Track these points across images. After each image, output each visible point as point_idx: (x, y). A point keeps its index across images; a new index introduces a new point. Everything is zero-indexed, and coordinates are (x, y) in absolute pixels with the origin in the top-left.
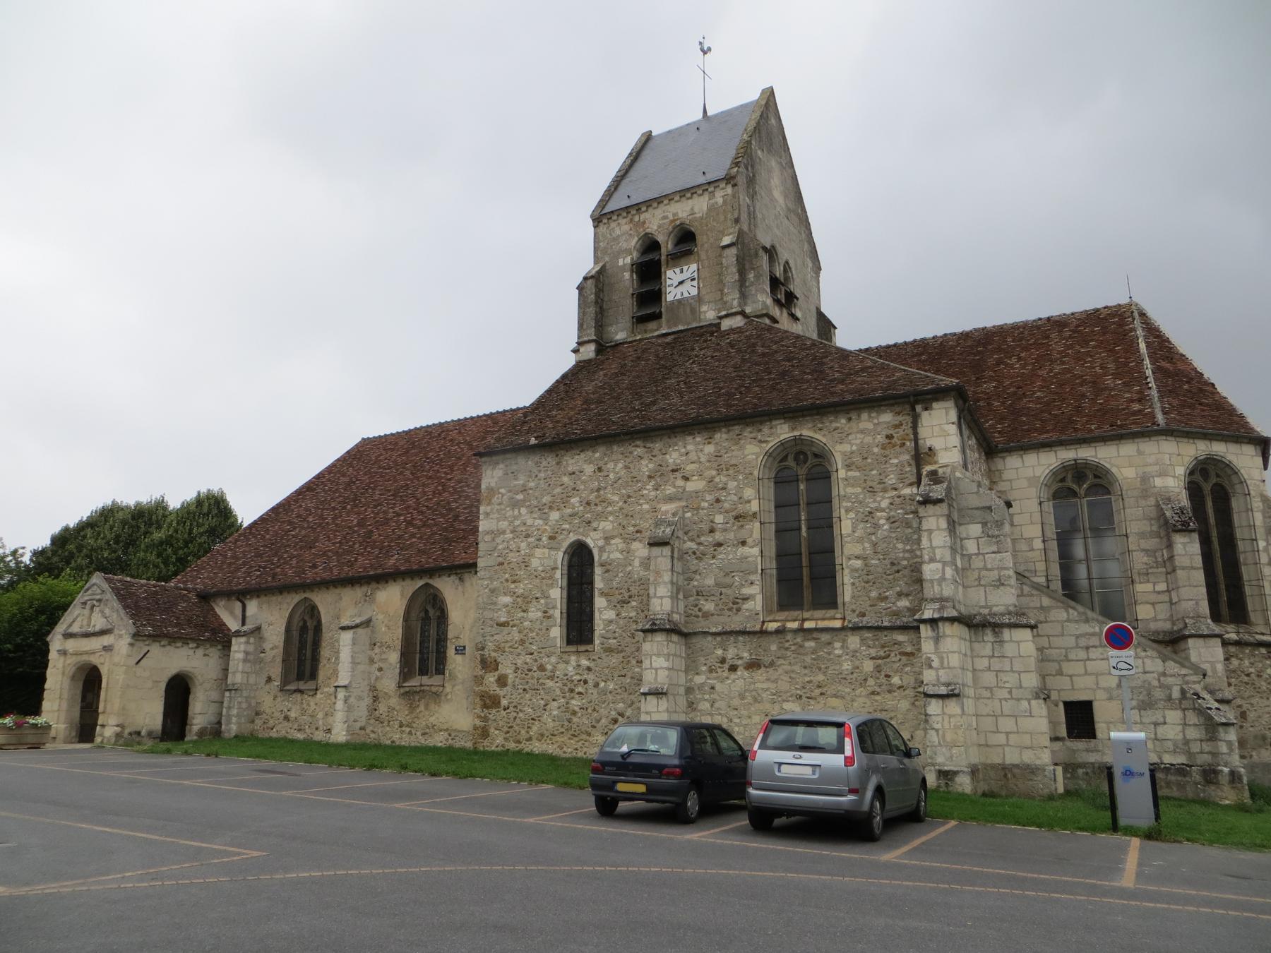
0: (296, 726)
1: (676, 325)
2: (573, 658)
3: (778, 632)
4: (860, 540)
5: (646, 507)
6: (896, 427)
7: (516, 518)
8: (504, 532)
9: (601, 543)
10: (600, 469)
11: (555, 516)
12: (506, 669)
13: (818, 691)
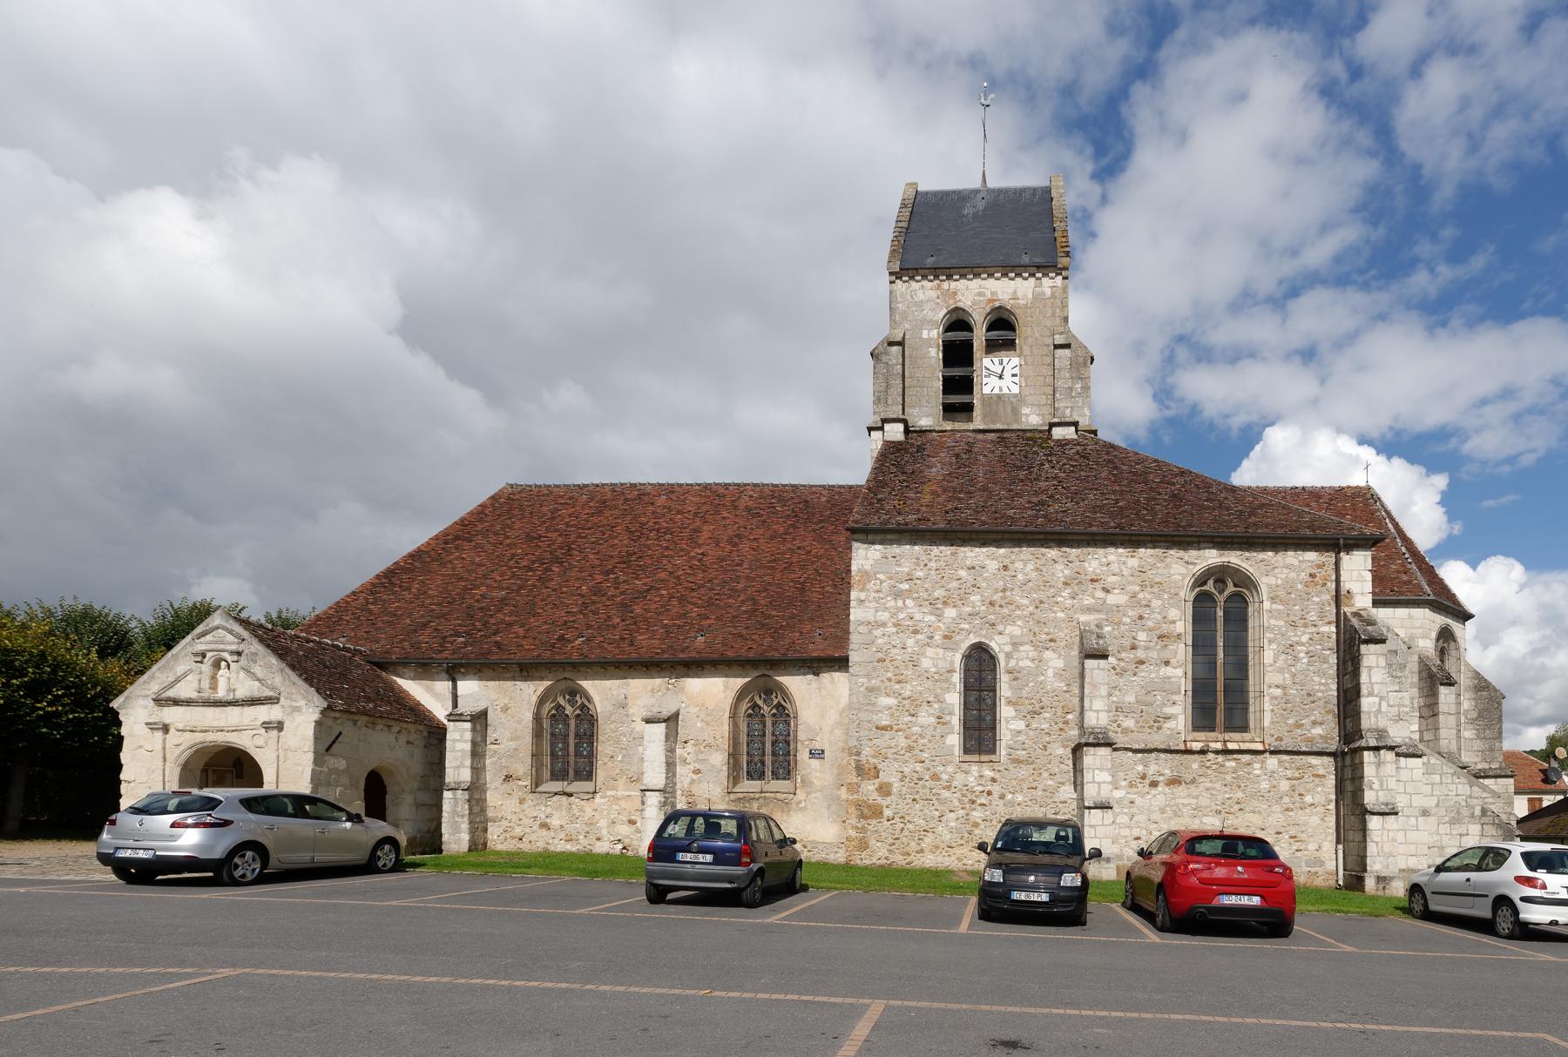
0: (562, 835)
1: (994, 422)
2: (974, 768)
3: (1202, 752)
4: (1281, 671)
5: (1060, 615)
6: (1320, 566)
7: (899, 610)
8: (884, 625)
9: (1008, 648)
10: (1005, 568)
11: (950, 613)
12: (889, 775)
13: (1237, 807)
